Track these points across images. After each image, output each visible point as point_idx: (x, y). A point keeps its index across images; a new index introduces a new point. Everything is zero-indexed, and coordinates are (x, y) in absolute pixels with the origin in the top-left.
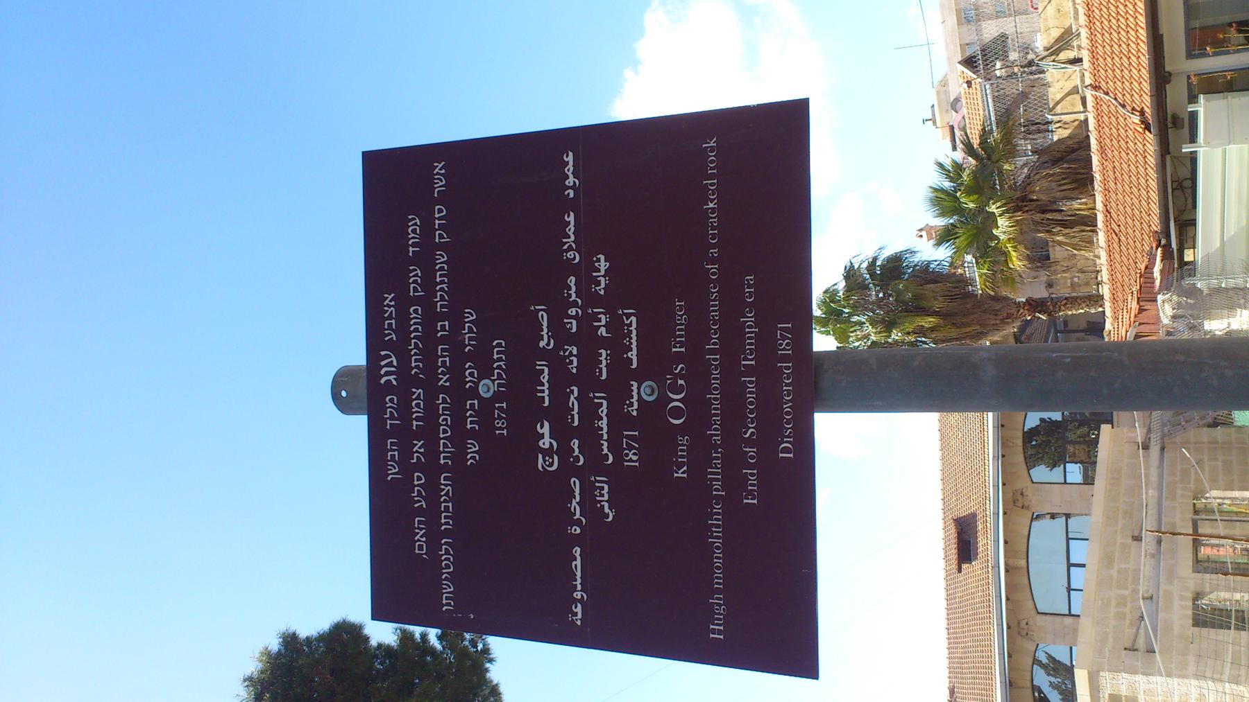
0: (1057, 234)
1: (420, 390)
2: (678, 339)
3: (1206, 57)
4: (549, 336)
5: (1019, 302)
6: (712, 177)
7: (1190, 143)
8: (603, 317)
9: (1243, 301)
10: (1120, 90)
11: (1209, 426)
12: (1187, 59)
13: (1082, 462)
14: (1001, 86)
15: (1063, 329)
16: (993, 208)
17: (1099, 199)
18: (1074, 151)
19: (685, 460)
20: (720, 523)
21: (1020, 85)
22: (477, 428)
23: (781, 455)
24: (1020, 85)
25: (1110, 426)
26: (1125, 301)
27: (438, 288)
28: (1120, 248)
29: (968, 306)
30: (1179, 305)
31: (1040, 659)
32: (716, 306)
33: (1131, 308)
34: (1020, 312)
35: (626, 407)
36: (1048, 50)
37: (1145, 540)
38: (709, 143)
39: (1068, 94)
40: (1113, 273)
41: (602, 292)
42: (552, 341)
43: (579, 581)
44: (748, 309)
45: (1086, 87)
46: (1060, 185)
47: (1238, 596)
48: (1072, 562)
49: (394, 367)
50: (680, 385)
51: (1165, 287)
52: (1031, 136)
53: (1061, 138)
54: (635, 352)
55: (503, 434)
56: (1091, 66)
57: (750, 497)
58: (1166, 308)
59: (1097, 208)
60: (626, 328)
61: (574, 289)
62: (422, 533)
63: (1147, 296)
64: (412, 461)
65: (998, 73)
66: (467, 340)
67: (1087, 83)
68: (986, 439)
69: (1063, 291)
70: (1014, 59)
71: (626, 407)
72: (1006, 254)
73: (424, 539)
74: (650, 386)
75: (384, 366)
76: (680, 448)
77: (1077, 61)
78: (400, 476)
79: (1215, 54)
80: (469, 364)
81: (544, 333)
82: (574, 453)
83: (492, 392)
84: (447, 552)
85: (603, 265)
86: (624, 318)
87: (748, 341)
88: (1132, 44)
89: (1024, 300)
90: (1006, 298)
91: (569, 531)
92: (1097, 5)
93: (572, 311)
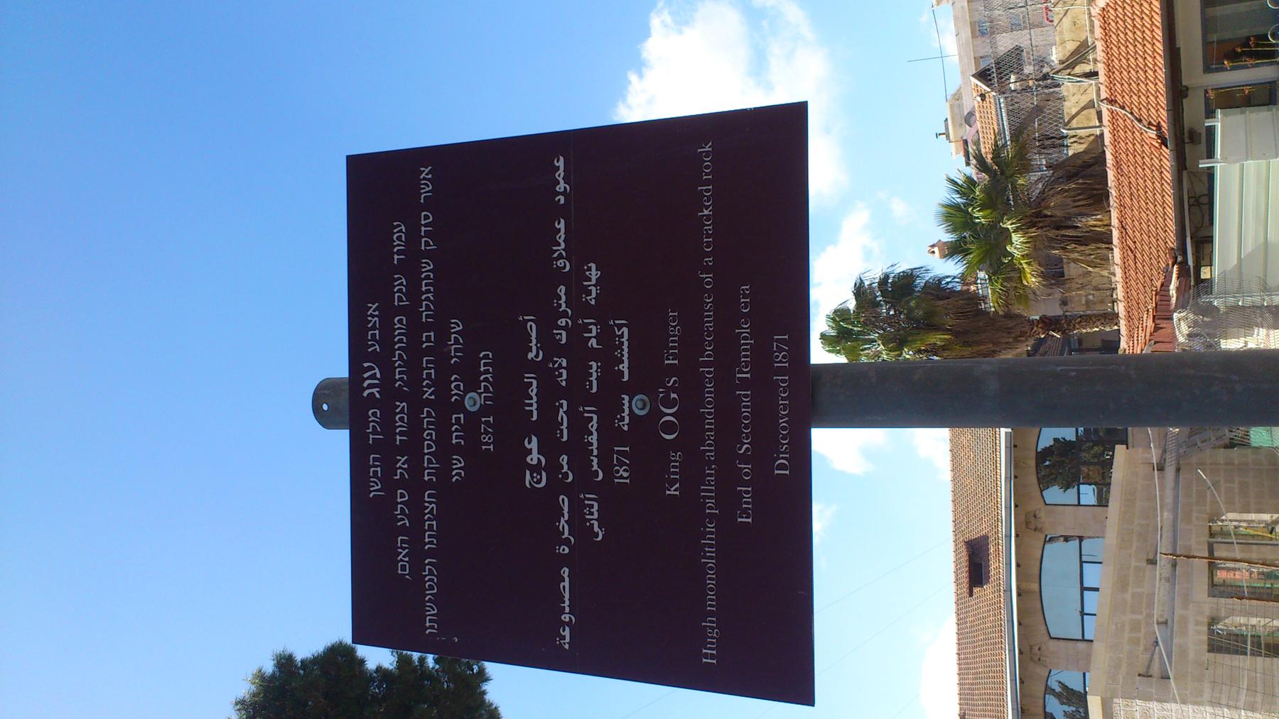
0: (1072, 251)
1: (404, 404)
2: (671, 351)
3: (1224, 71)
4: (537, 347)
5: (1033, 321)
6: (707, 182)
7: (1208, 158)
8: (593, 328)
9: (1261, 319)
10: (1137, 104)
11: (1226, 447)
12: (1204, 73)
13: (1095, 484)
14: (1016, 100)
15: (1077, 347)
16: (1009, 225)
17: (1114, 214)
19: (678, 477)
20: (714, 542)
21: (1035, 98)
22: (463, 443)
23: (776, 472)
24: (1035, 98)
25: (1125, 446)
27: (423, 297)
28: (1135, 264)
29: (981, 324)
30: (1195, 323)
31: (1053, 688)
32: (710, 316)
33: (1146, 326)
34: (1034, 331)
35: (616, 421)
36: (1063, 63)
37: (1160, 564)
38: (704, 148)
39: (1084, 108)
40: (1129, 290)
41: (593, 302)
42: (541, 353)
43: (567, 603)
44: (743, 320)
45: (1102, 101)
46: (1075, 201)
47: (1254, 621)
48: (1085, 585)
49: (378, 379)
50: (674, 398)
51: (1181, 305)
52: (1045, 151)
53: (1076, 152)
55: (490, 449)
56: (1107, 80)
57: (744, 516)
58: (1182, 327)
59: (1113, 224)
60: (617, 339)
61: (564, 298)
62: (404, 552)
63: (1162, 314)
64: (395, 478)
65: (1012, 86)
66: (453, 352)
67: (1102, 97)
68: (998, 459)
69: (1077, 308)
70: (1029, 72)
71: (616, 421)
72: (1020, 271)
73: (407, 559)
74: (642, 400)
75: (368, 378)
76: (673, 464)
77: (1093, 74)
78: (383, 493)
79: (1233, 68)
80: (454, 376)
82: (563, 469)
83: (478, 406)
84: (431, 573)
85: (594, 274)
86: (616, 329)
87: (743, 353)
88: (1148, 58)
89: (1038, 318)
91: (557, 551)
92: (1113, 18)
93: (562, 322)
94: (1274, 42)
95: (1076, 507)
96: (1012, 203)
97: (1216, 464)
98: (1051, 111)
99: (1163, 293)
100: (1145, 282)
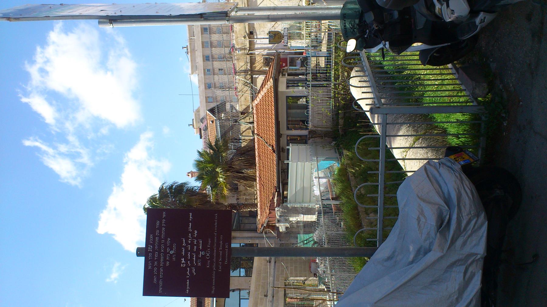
7: (287, 160)
16: (218, 170)
18: (249, 151)
26: (265, 209)
39: (247, 129)
51: (278, 205)
54: (201, 246)
61: (190, 236)
63: (272, 209)
69: (242, 201)
81: (184, 243)
85: (196, 232)
90: (222, 204)
93: (190, 239)
94: (307, 125)
95: (239, 277)
96: (221, 161)
97: (287, 260)
98: (236, 129)
99: (272, 201)
100: (267, 196)
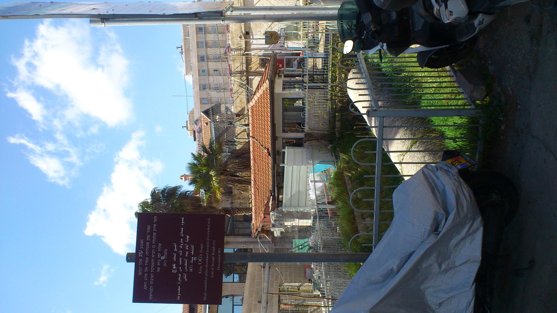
7: (283, 163)
16: (212, 173)
18: (244, 154)
26: (259, 213)
28: (259, 194)
39: (243, 132)
46: (238, 166)
51: (273, 210)
61: (182, 241)
63: (266, 213)
81: (175, 248)
85: (188, 237)
93: (181, 245)
94: (303, 127)
96: (215, 164)
